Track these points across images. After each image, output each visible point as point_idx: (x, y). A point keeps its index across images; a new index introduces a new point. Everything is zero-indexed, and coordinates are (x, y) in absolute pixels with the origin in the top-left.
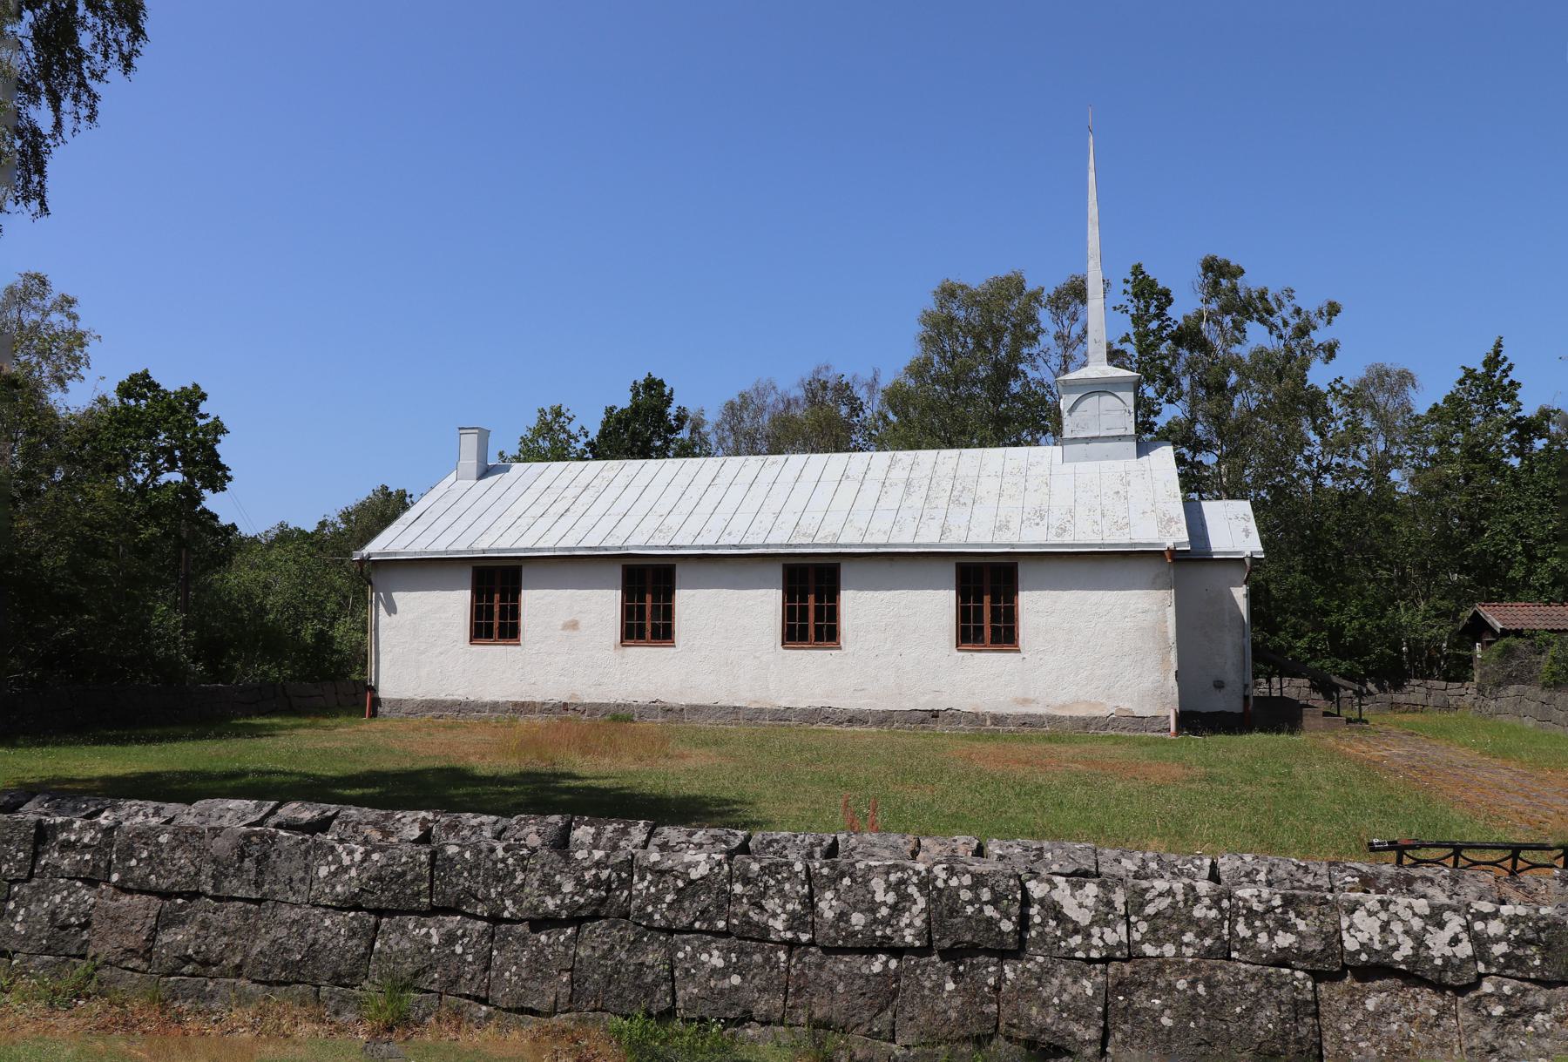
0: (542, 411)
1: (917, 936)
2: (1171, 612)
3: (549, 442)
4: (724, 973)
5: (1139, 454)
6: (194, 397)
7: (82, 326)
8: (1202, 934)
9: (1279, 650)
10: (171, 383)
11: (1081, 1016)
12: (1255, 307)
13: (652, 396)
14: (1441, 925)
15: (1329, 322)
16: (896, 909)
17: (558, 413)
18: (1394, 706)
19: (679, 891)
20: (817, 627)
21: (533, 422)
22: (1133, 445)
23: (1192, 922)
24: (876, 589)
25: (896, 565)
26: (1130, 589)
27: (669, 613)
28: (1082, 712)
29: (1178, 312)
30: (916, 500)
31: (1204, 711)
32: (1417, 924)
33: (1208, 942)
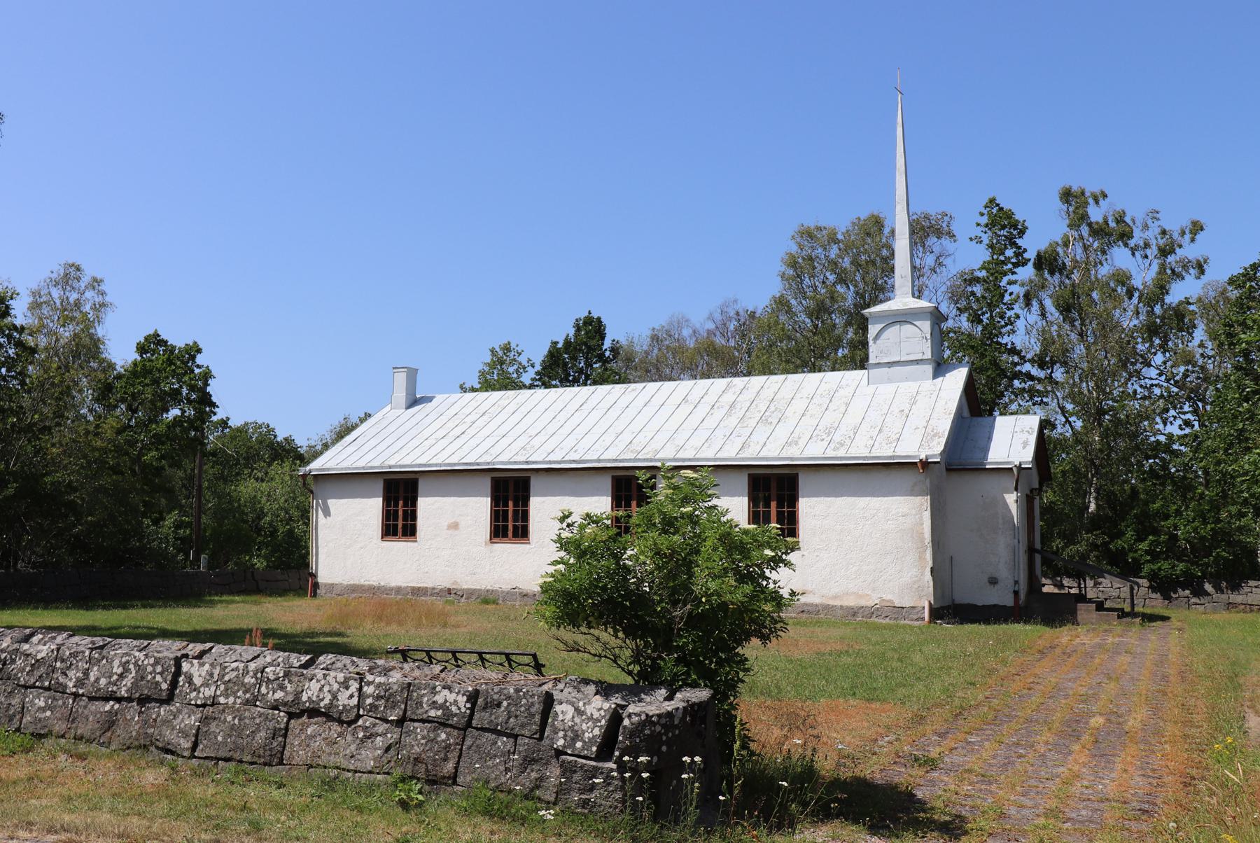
0: (493, 351)
1: (127, 691)
2: (927, 515)
3: (500, 375)
4: (43, 710)
5: (935, 376)
6: (193, 351)
7: (108, 299)
8: (245, 692)
9: (1123, 552)
10: (178, 339)
11: (186, 736)
12: (1116, 232)
13: (592, 329)
14: (347, 688)
15: (1193, 240)
16: (121, 676)
17: (507, 348)
18: (1230, 606)
19: (32, 665)
20: (514, 526)
21: (488, 358)
22: (929, 369)
23: (243, 684)
24: (836, 496)
25: (454, 478)
26: (893, 496)
27: (525, 516)
28: (851, 602)
29: (1033, 244)
30: (733, 420)
31: (980, 604)
32: (336, 686)
33: (248, 696)
